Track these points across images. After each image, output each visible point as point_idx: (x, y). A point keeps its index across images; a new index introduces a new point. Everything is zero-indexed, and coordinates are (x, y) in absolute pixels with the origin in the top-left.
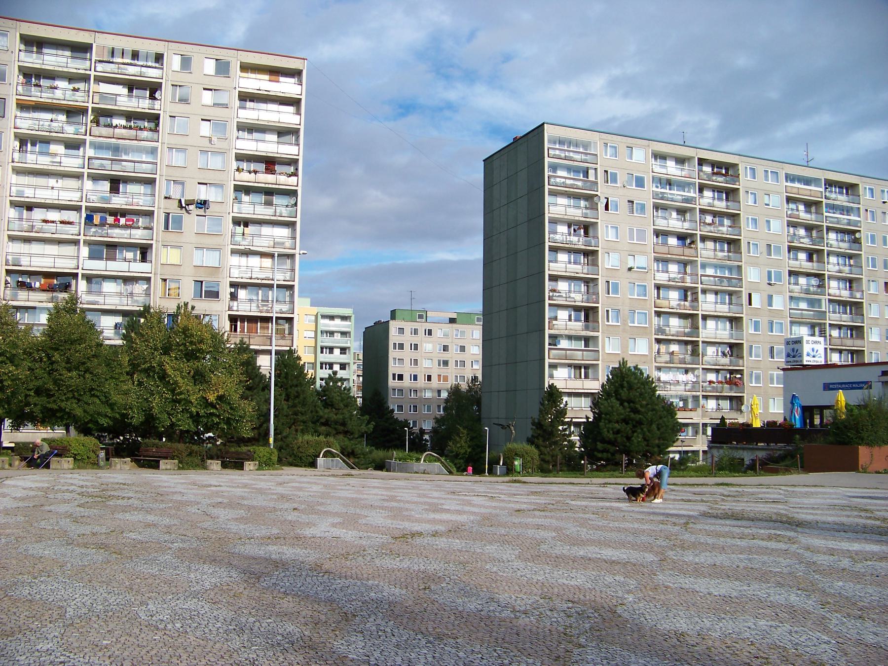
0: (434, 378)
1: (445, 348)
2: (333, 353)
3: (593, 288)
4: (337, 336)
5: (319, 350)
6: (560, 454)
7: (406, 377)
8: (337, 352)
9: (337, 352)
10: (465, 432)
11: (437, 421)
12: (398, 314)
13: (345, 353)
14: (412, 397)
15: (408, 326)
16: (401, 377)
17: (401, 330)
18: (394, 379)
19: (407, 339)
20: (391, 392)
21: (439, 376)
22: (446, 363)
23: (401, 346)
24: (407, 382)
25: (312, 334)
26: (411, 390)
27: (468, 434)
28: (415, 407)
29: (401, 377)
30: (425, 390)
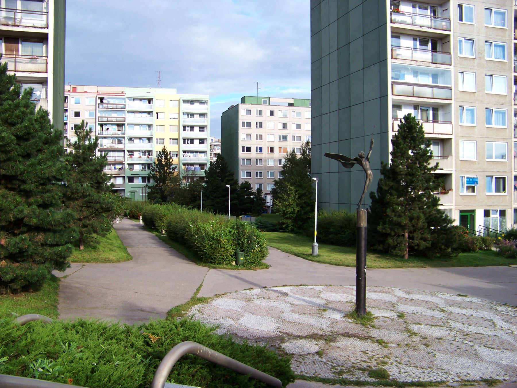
0: (276, 150)
1: (285, 126)
2: (193, 131)
3: (441, 14)
4: (197, 117)
5: (182, 128)
6: (422, 215)
7: (253, 149)
8: (197, 129)
9: (197, 129)
10: (292, 188)
11: (276, 183)
12: (246, 100)
13: (203, 131)
14: (258, 165)
15: (255, 109)
16: (249, 149)
17: (249, 112)
18: (243, 151)
19: (254, 118)
20: (240, 161)
21: (280, 148)
22: (285, 138)
23: (249, 124)
24: (254, 154)
25: (176, 116)
26: (257, 160)
27: (296, 191)
28: (261, 173)
29: (249, 149)
30: (268, 159)
